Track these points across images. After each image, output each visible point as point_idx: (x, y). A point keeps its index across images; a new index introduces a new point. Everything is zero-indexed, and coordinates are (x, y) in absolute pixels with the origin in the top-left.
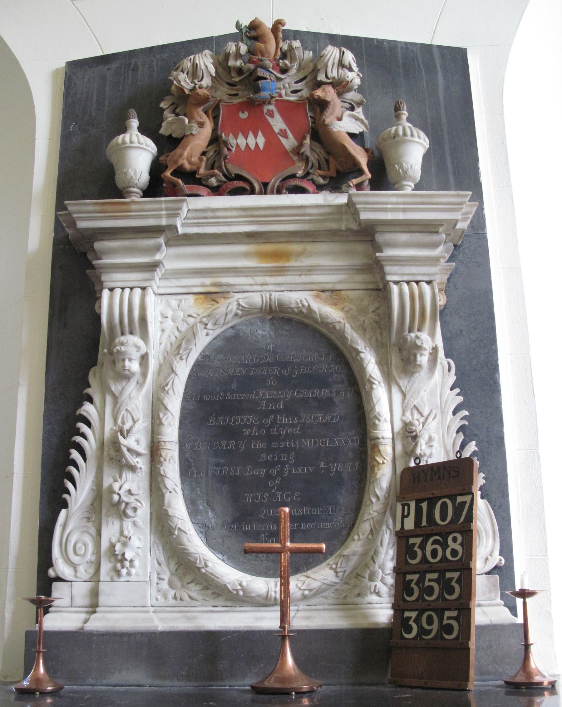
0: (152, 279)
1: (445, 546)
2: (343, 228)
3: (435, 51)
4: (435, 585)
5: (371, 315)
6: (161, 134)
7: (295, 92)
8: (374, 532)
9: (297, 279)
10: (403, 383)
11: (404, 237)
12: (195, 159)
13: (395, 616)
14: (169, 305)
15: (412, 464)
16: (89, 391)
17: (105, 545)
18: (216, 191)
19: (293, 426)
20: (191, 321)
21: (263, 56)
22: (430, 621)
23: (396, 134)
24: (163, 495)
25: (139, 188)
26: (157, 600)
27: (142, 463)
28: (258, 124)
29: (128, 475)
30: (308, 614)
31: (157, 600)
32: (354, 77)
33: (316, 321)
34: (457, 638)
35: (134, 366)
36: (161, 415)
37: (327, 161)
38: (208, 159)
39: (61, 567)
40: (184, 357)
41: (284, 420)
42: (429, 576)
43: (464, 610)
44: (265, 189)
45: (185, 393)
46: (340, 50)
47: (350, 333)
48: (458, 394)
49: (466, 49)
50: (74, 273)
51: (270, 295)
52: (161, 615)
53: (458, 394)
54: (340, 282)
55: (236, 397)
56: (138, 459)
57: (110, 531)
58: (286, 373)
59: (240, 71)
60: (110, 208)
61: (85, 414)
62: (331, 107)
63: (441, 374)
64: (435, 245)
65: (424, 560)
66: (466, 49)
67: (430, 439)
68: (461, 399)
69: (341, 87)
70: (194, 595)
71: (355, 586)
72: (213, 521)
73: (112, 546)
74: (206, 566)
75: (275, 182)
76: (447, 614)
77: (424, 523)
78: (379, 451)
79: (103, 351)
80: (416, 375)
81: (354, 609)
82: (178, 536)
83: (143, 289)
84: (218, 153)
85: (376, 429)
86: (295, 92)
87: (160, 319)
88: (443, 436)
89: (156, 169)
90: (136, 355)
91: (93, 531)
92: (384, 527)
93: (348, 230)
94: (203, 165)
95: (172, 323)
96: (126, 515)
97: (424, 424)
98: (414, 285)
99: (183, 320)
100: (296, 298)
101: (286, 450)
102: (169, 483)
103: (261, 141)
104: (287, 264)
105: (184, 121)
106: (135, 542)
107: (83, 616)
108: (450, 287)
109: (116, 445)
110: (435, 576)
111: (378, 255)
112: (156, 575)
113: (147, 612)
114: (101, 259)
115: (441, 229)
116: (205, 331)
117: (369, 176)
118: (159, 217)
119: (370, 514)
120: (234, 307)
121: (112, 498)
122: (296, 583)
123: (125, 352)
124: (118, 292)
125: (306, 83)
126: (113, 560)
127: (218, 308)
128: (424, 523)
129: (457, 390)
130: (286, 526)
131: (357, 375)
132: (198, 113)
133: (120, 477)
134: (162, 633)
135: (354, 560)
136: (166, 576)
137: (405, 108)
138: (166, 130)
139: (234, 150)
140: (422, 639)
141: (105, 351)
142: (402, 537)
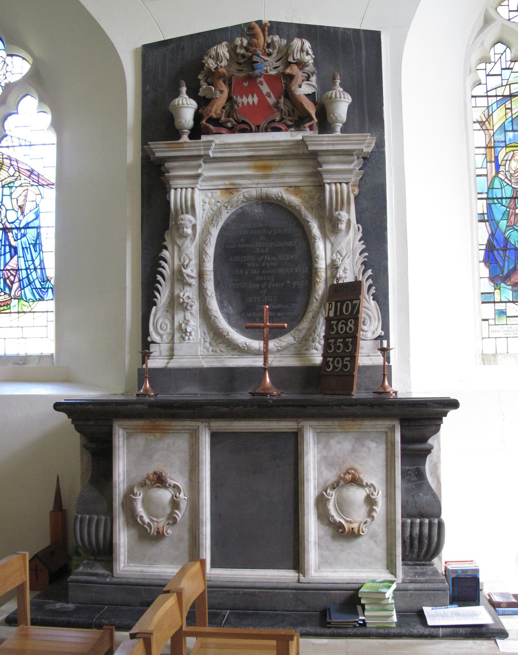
0: (197, 183)
1: (346, 325)
2: (301, 153)
3: (361, 33)
4: (341, 345)
5: (316, 200)
6: (199, 96)
7: (275, 68)
8: (315, 317)
9: (276, 181)
10: (332, 238)
11: (333, 158)
12: (219, 112)
13: (323, 360)
14: (206, 195)
15: (335, 283)
16: (165, 243)
17: (176, 324)
18: (232, 130)
19: (274, 261)
20: (219, 204)
21: (256, 48)
22: (338, 363)
23: (331, 97)
24: (206, 299)
25: (188, 129)
26: (204, 352)
27: (194, 282)
28: (254, 89)
29: (188, 288)
30: (280, 359)
31: (204, 352)
32: (309, 59)
33: (286, 204)
34: (349, 370)
35: (189, 231)
36: (204, 257)
37: (293, 111)
38: (226, 111)
39: (154, 336)
40: (216, 225)
41: (269, 259)
42: (339, 340)
43: (353, 357)
44: (258, 130)
45: (216, 245)
46: (302, 41)
47: (304, 211)
48: (363, 244)
49: (380, 32)
50: (155, 180)
51: (261, 190)
52: (205, 360)
53: (363, 244)
54: (299, 182)
55: (243, 246)
56: (192, 280)
57: (179, 318)
58: (270, 233)
59: (243, 56)
60: (173, 146)
61: (163, 256)
62: (295, 78)
63: (354, 233)
64: (351, 162)
65: (337, 332)
66: (380, 32)
67: (345, 269)
68: (364, 246)
69: (301, 64)
70: (223, 349)
71: (304, 345)
72: (232, 311)
73: (180, 325)
74: (228, 335)
75: (263, 125)
76: (346, 359)
77: (338, 314)
78: (318, 275)
79: (172, 223)
80: (339, 234)
81: (304, 357)
82: (214, 320)
83: (193, 188)
84: (232, 107)
85: (317, 264)
86: (275, 68)
87: (202, 203)
88: (353, 267)
89: (198, 117)
90: (190, 225)
91: (170, 317)
92: (320, 315)
93: (303, 154)
94: (224, 114)
95: (209, 206)
96: (187, 309)
97: (342, 261)
98: (338, 185)
99: (214, 204)
100: (276, 191)
101: (270, 275)
102: (209, 293)
103: (256, 99)
104: (270, 173)
105: (211, 89)
106: (192, 323)
107: (167, 361)
108: (361, 184)
109: (181, 273)
110: (341, 340)
111: (319, 169)
112: (203, 340)
113: (199, 358)
114: (169, 173)
115: (354, 153)
116: (226, 211)
117: (316, 120)
118: (200, 150)
119: (312, 308)
120: (241, 197)
121: (179, 301)
122: (272, 344)
123: (184, 224)
124: (179, 190)
125: (282, 62)
126: (181, 332)
127: (232, 198)
128: (338, 314)
129: (362, 242)
130: (266, 315)
131: (308, 234)
132: (220, 83)
133: (184, 290)
134: (207, 368)
135: (304, 332)
136: (208, 340)
137: (339, 77)
138: (202, 93)
139: (240, 105)
140: (334, 371)
141: (173, 223)
142: (328, 320)
